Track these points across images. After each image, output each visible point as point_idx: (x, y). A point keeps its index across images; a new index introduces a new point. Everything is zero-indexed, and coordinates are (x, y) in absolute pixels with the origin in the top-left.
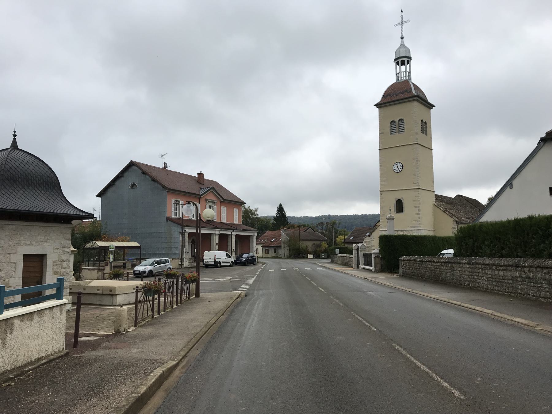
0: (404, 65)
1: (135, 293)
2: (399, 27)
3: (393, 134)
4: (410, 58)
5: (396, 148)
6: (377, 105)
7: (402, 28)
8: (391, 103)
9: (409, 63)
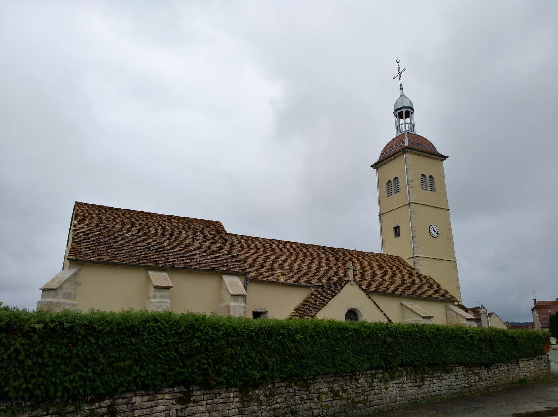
0: (409, 117)
1: (385, 321)
2: (398, 78)
4: (413, 110)
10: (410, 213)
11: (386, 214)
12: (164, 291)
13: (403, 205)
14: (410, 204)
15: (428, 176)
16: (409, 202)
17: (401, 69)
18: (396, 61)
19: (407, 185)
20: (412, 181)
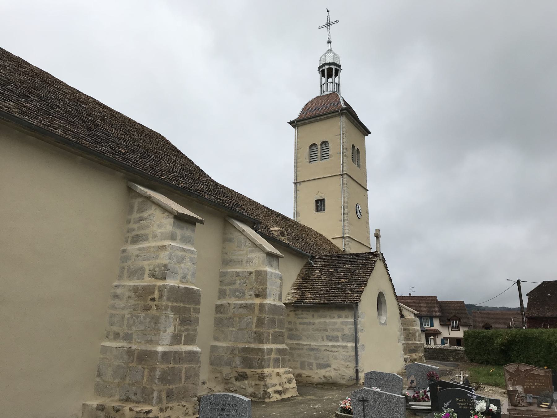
3: (312, 162)
5: (316, 180)
6: (294, 123)
7: (329, 32)
9: (339, 74)
10: (343, 185)
11: (306, 182)
12: (187, 229)
13: (334, 175)
14: (343, 175)
16: (343, 173)
17: (332, 20)
19: (341, 152)
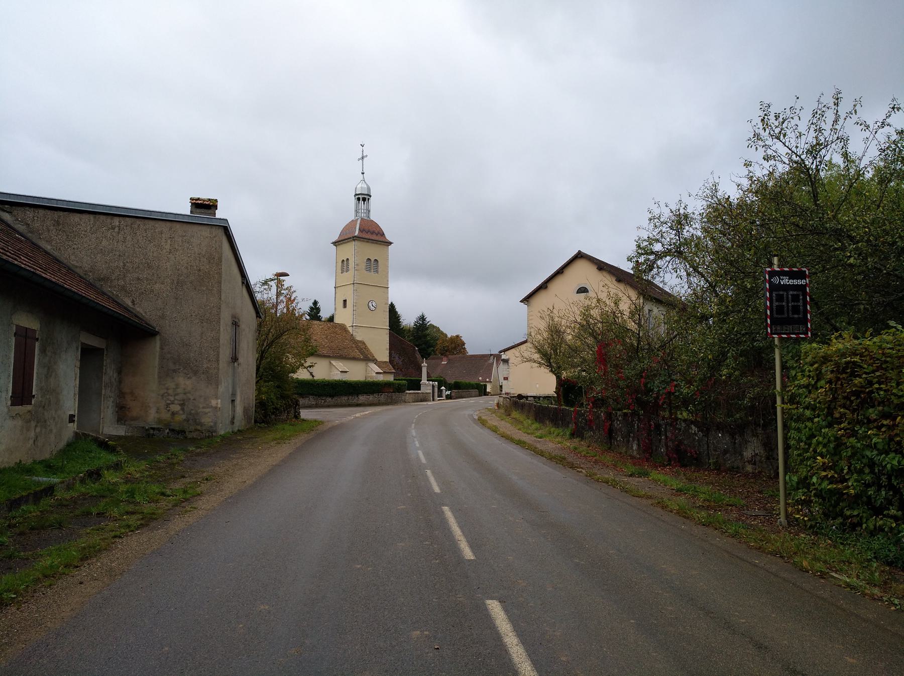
1: (311, 377)
2: (365, 155)
4: (370, 196)
8: (344, 241)
15: (373, 260)
18: (361, 145)
20: (357, 265)
